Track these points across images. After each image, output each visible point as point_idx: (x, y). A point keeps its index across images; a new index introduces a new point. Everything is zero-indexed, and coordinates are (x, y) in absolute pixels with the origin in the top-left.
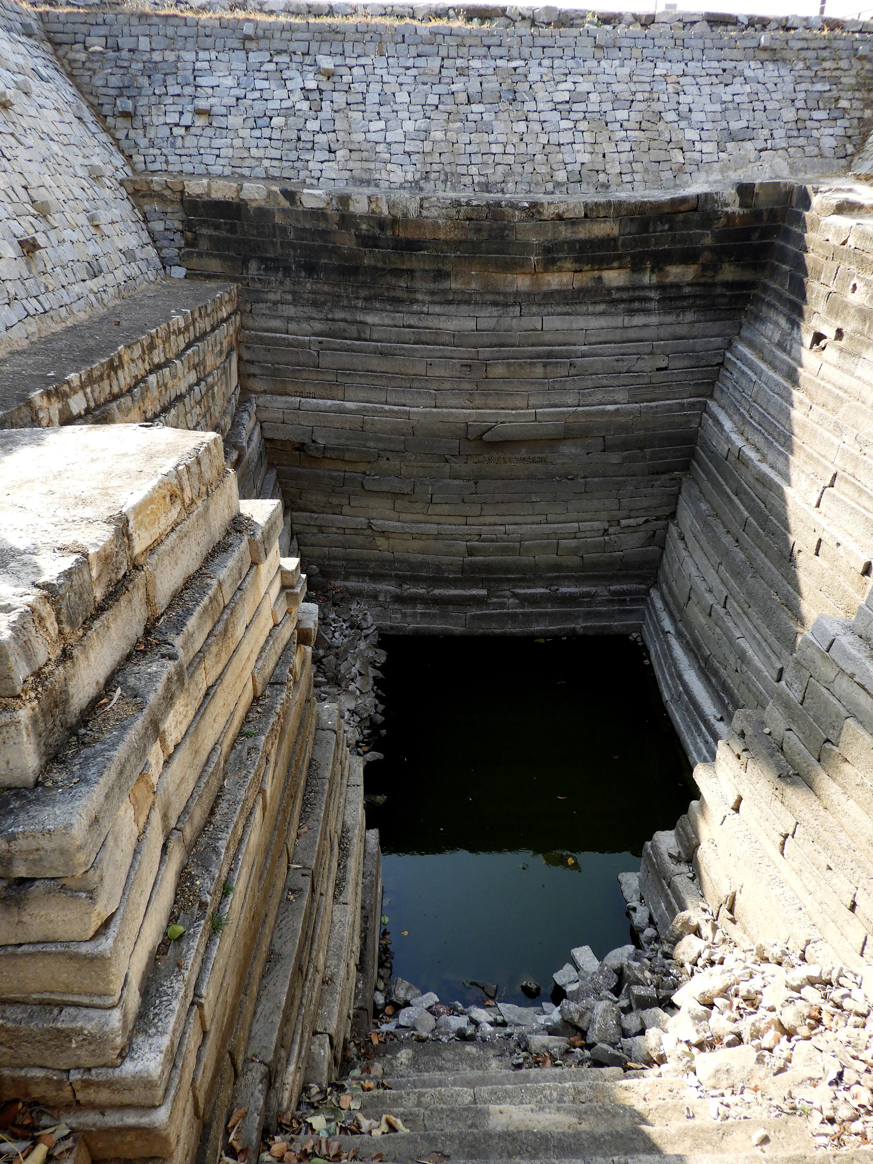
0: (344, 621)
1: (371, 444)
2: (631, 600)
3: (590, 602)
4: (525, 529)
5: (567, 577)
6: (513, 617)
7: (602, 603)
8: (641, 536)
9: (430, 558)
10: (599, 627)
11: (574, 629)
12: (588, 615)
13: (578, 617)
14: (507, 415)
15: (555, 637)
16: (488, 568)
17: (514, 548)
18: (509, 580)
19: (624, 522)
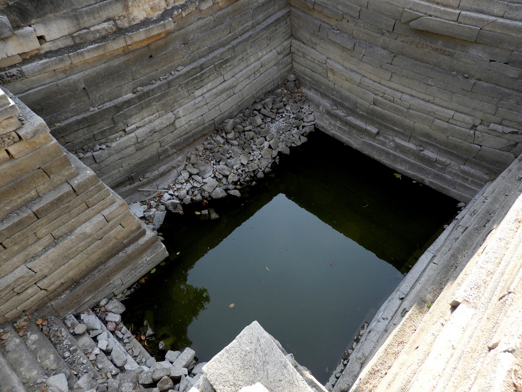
0: (293, 114)
1: (340, 7)
2: (472, 181)
3: (441, 169)
4: (414, 102)
5: (433, 145)
6: (388, 154)
7: (450, 173)
8: (503, 142)
9: (352, 97)
10: (441, 187)
11: (423, 180)
12: (436, 176)
13: (429, 174)
14: (436, 10)
15: (406, 179)
16: (382, 117)
17: (402, 111)
18: (394, 130)
19: (492, 126)
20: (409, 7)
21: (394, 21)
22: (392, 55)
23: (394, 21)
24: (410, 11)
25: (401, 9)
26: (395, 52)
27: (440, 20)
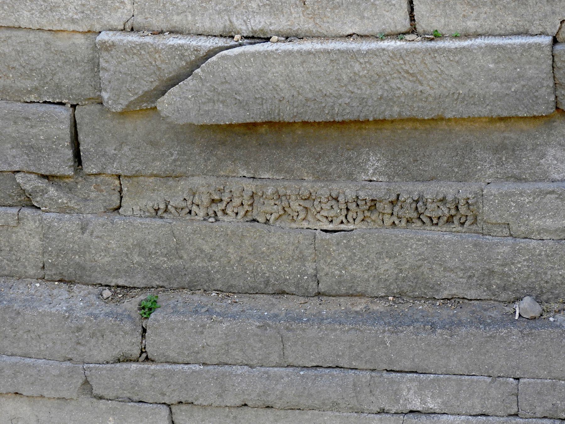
20: (117, 19)
21: (64, 113)
22: (131, 305)
23: (64, 113)
24: (133, 38)
25: (80, 40)
26: (139, 281)
27: (317, 45)
